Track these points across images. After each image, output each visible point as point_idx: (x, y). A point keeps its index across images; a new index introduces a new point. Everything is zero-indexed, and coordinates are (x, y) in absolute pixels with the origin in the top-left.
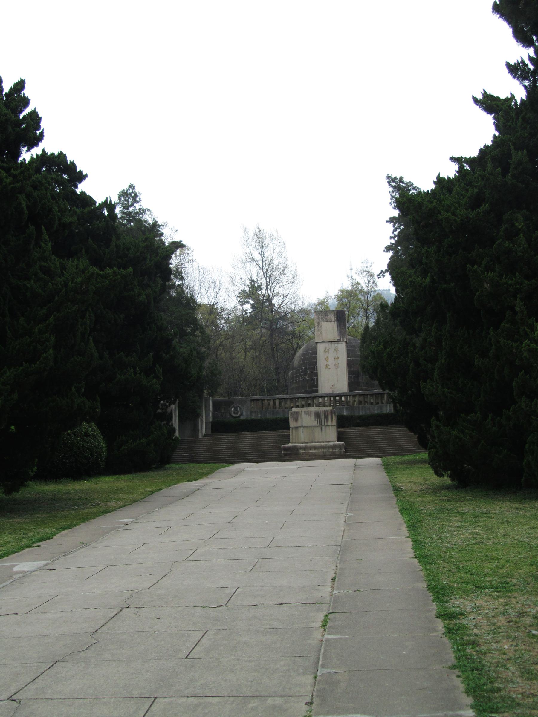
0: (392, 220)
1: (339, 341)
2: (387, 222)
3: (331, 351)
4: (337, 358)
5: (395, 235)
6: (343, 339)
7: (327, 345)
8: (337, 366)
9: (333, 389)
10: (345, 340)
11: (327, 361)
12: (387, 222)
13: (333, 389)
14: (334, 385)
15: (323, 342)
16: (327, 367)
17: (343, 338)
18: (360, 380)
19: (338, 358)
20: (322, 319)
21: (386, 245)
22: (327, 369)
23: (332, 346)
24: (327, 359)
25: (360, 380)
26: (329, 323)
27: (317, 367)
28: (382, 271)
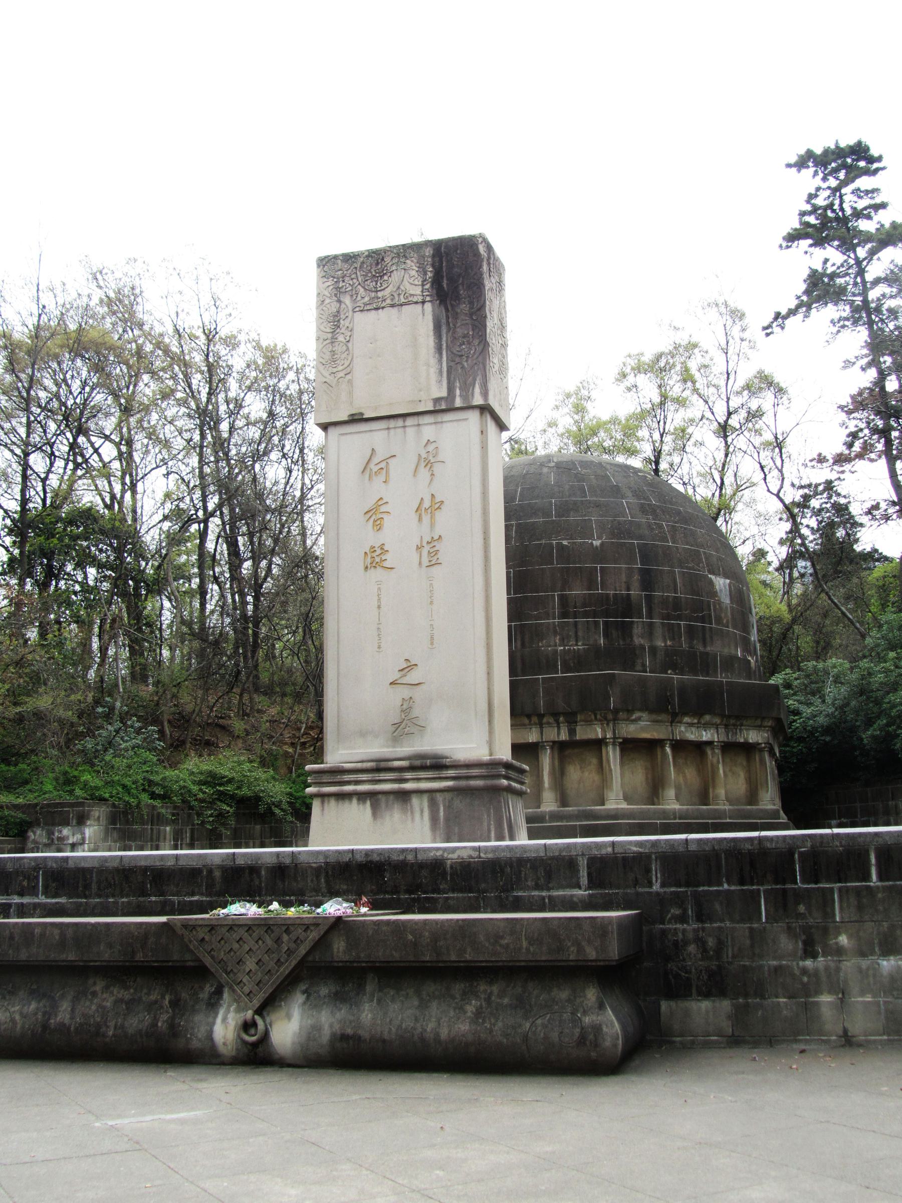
0: (799, 171)
1: (442, 408)
2: (789, 166)
3: (400, 469)
4: (429, 509)
5: (814, 206)
6: (465, 397)
7: (376, 438)
8: (434, 553)
9: (406, 692)
10: (478, 400)
11: (378, 526)
12: (789, 166)
13: (406, 692)
14: (410, 666)
15: (356, 419)
16: (375, 559)
17: (467, 390)
18: (638, 641)
19: (436, 505)
20: (354, 295)
21: (785, 234)
22: (377, 574)
23: (408, 442)
24: (375, 515)
25: (638, 641)
26: (394, 311)
27: (508, 593)
28: (778, 315)
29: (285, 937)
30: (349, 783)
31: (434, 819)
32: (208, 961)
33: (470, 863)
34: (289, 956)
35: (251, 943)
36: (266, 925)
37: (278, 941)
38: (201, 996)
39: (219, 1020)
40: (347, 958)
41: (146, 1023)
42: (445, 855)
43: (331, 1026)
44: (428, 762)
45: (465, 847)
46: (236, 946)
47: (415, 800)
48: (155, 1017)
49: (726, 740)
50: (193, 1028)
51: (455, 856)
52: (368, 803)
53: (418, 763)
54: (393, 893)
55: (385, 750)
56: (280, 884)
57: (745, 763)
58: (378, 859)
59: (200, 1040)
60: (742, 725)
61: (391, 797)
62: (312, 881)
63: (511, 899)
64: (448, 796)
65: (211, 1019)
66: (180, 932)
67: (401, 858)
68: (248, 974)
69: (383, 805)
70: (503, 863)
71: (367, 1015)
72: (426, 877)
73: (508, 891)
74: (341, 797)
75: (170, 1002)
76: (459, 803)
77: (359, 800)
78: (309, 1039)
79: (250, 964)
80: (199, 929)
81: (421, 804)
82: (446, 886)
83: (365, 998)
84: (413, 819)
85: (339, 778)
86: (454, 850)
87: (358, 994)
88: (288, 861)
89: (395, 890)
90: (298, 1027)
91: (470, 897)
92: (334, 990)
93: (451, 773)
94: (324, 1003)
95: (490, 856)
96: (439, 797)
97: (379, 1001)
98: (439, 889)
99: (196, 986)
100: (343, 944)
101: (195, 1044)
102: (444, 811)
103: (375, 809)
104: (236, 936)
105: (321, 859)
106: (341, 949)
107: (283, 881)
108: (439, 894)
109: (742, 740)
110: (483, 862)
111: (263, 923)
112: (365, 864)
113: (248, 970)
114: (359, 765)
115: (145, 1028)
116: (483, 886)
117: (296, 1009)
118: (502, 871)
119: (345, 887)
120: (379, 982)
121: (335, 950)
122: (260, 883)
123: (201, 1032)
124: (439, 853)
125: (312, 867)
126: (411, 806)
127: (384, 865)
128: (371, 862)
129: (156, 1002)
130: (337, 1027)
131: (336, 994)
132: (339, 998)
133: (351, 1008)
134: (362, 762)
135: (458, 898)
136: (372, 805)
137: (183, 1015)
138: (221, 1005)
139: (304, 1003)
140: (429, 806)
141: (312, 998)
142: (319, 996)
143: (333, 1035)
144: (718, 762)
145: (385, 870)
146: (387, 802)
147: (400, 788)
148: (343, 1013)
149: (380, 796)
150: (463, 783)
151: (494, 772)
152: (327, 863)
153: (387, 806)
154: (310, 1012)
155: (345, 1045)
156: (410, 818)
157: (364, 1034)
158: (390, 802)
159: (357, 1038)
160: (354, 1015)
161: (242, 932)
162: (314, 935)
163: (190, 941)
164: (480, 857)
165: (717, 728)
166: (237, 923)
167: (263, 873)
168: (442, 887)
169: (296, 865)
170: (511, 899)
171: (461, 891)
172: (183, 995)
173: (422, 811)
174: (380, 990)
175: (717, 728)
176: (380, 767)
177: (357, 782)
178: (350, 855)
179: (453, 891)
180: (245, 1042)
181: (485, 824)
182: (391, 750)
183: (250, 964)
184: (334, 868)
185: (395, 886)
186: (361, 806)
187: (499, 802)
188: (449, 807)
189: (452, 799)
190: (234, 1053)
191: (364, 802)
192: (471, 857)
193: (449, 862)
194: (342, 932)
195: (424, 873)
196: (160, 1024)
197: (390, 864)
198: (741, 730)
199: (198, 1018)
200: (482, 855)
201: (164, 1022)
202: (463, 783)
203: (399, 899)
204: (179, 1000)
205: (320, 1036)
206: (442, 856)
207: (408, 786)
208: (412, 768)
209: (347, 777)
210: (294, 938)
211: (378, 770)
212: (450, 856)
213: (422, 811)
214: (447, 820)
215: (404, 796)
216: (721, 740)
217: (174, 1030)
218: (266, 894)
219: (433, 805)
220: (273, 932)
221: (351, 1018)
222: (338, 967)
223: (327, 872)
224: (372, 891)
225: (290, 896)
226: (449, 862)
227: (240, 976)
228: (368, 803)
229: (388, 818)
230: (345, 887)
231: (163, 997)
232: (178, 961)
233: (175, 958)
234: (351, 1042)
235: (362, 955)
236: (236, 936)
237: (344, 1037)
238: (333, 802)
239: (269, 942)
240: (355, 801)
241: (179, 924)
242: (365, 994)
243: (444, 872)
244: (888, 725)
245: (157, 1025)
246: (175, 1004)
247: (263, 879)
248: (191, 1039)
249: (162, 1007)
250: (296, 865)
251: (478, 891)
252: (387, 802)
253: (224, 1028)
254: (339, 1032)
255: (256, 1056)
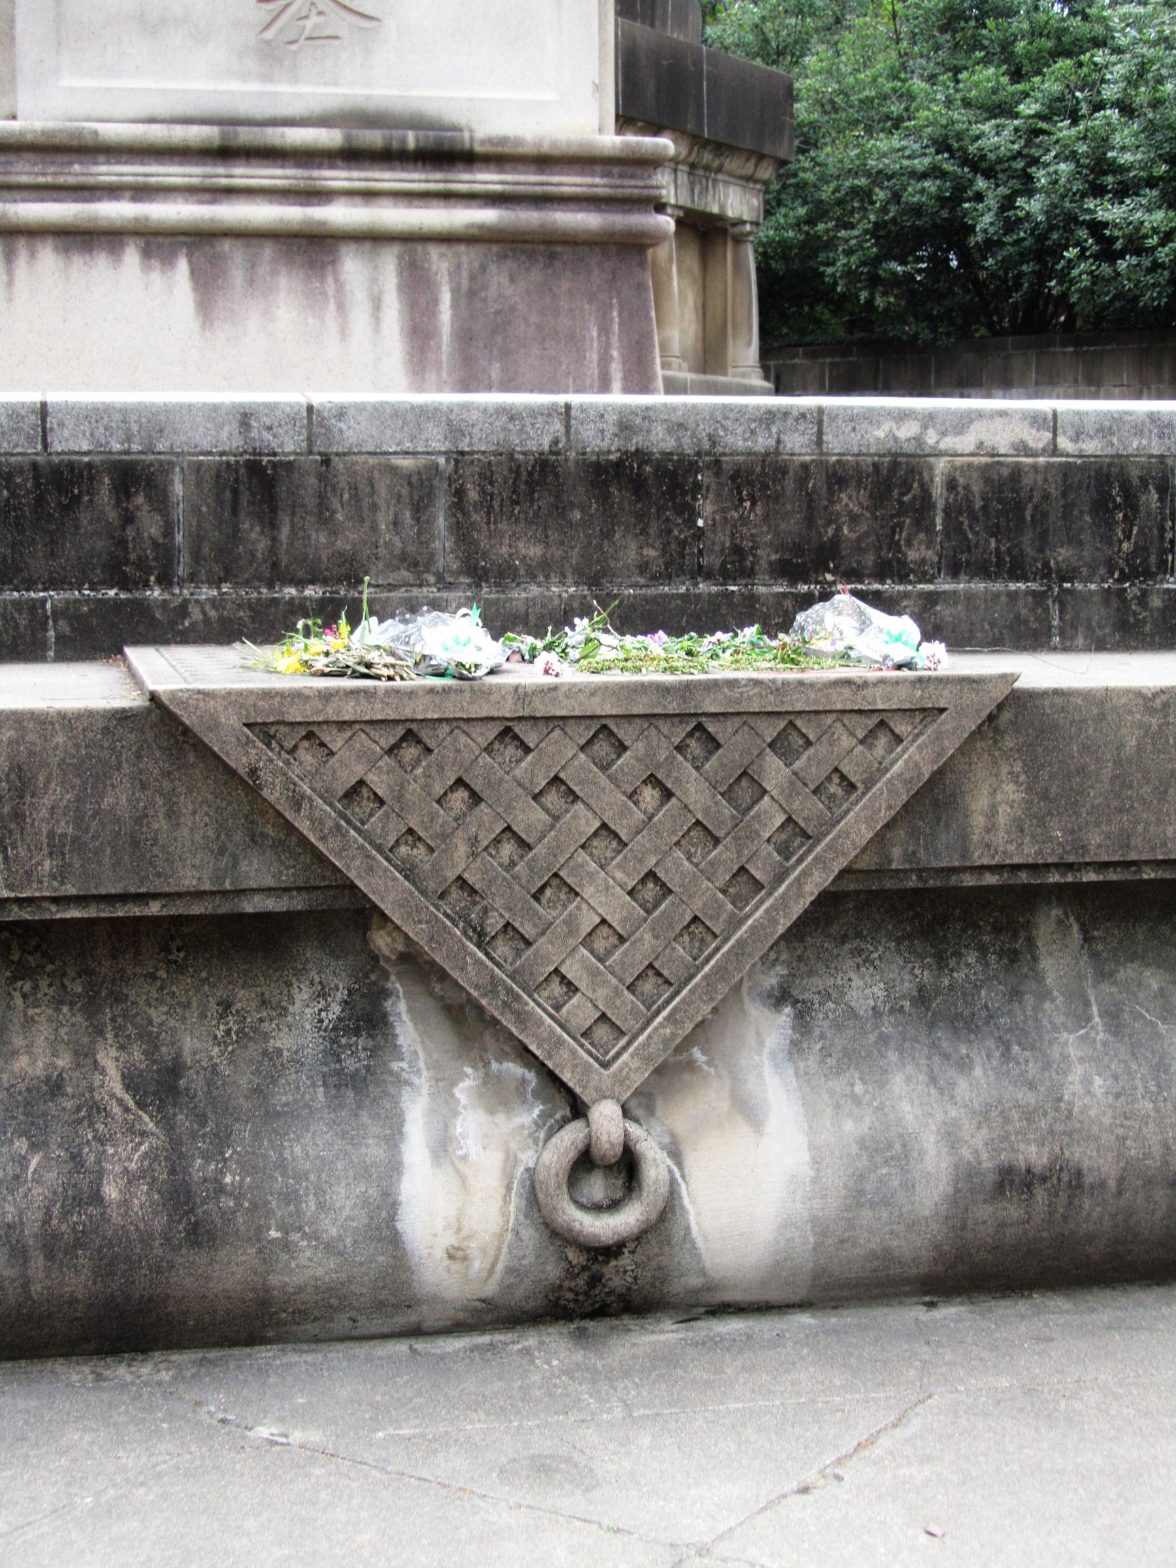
29: (774, 772)
30: (113, 191)
31: (419, 334)
32: (384, 888)
33: (1017, 472)
34: (785, 851)
35: (606, 799)
36: (682, 717)
37: (744, 785)
38: (284, 1041)
39: (416, 1148)
40: (1028, 853)
41: (39, 1193)
42: (931, 438)
43: (950, 1136)
44: (411, 140)
45: (1003, 414)
46: (529, 818)
47: (353, 266)
48: (76, 1158)
49: (689, 204)
50: (290, 1197)
51: (965, 443)
52: (183, 266)
53: (373, 138)
54: (726, 576)
55: (236, 86)
56: (255, 538)
57: (696, 268)
58: (670, 444)
59: (329, 1247)
60: (719, 170)
61: (268, 251)
62: (396, 523)
63: (1156, 602)
64: (469, 256)
65: (374, 1151)
66: (239, 761)
67: (763, 442)
68: (588, 941)
69: (237, 275)
70: (1135, 473)
71: (1087, 1081)
72: (854, 519)
73: (1148, 575)
74: (80, 239)
75: (131, 1082)
76: (504, 283)
77: (147, 253)
78: (857, 1197)
79: (604, 896)
80: (336, 740)
81: (374, 281)
82: (930, 555)
83: (1054, 1009)
84: (344, 333)
85: (77, 172)
86: (963, 422)
87: (1015, 994)
88: (289, 444)
89: (738, 564)
90: (806, 1157)
91: (1013, 596)
92: (907, 986)
93: (488, 180)
94: (884, 1039)
95: (1092, 447)
96: (439, 261)
97: (1113, 1015)
98: (903, 563)
99: (244, 998)
100: (1011, 792)
101: (306, 1268)
102: (455, 305)
103: (207, 284)
104: (531, 770)
105: (436, 440)
106: (1004, 816)
107: (272, 525)
108: (903, 579)
109: (715, 210)
110: (1066, 471)
111: (673, 706)
112: (619, 464)
113: (588, 921)
114: (158, 133)
115: (34, 1216)
116: (1063, 554)
117: (768, 1069)
118: (1131, 502)
119: (535, 551)
120: (1087, 939)
121: (978, 821)
122: (168, 532)
123: (341, 1207)
124: (907, 431)
125: (394, 470)
126: (340, 286)
127: (693, 467)
128: (641, 455)
129: (55, 1086)
130: (977, 1145)
131: (922, 998)
132: (939, 1016)
133: (1006, 1055)
134: (152, 120)
135: (970, 597)
136: (194, 273)
137: (222, 1139)
138: (401, 1082)
139: (796, 1048)
140: (400, 288)
141: (821, 1024)
142: (852, 1013)
143: (966, 1175)
144: (670, 260)
145: (697, 487)
146: (252, 266)
147: (309, 222)
148: (979, 1081)
149: (226, 245)
150: (528, 217)
151: (631, 186)
152: (459, 457)
153: (251, 282)
154: (838, 1085)
155: (1014, 1212)
156: (332, 325)
157: (1097, 1160)
158: (263, 270)
159: (1070, 1181)
160: (1032, 1086)
161: (563, 753)
162: (912, 759)
163: (297, 803)
164: (1054, 451)
165: (675, 171)
166: (542, 709)
167: (178, 489)
168: (912, 555)
169: (326, 461)
170: (1156, 602)
171: (983, 571)
172: (188, 1044)
173: (377, 305)
174: (1103, 975)
175: (675, 171)
176: (232, 147)
177: (143, 192)
178: (557, 427)
179: (955, 571)
180: (558, 1236)
181: (593, 356)
182: (255, 87)
183: (604, 896)
184: (487, 476)
185: (738, 550)
186: (156, 276)
187: (641, 287)
188: (472, 294)
189: (483, 269)
190: (491, 1289)
191: (168, 261)
192: (1022, 448)
193: (941, 466)
194: (1009, 742)
195: (849, 501)
196: (111, 1192)
197: (716, 465)
198: (715, 181)
199: (311, 1146)
200: (1064, 443)
201: (132, 1179)
202: (528, 217)
203: (752, 599)
204: (175, 1069)
205: (909, 1187)
206: (919, 440)
207: (339, 215)
208: (351, 156)
209: (107, 172)
210: (817, 774)
211: (225, 153)
212: (949, 443)
213: (377, 305)
214: (464, 337)
215: (314, 248)
216: (681, 203)
217: (191, 1218)
218: (192, 578)
219: (416, 284)
220: (713, 744)
221: (1028, 1098)
222: (903, 893)
223: (460, 493)
224: (643, 568)
225: (300, 584)
226: (941, 466)
227: (549, 952)
228: (183, 266)
229: (254, 321)
230: (535, 551)
231: (85, 1057)
232: (199, 895)
233: (188, 880)
234: (1040, 1195)
235: (1094, 839)
236: (531, 770)
237: (1012, 1181)
238: (48, 256)
239: (695, 790)
240: (131, 256)
241: (232, 720)
242: (1044, 995)
243: (925, 503)
244: (811, 221)
245: (97, 1198)
246: (160, 1087)
247: (179, 512)
248: (286, 1246)
249: (96, 1109)
250: (326, 461)
251: (1046, 573)
252: (252, 266)
253: (454, 1173)
254: (987, 1163)
255: (598, 1287)
